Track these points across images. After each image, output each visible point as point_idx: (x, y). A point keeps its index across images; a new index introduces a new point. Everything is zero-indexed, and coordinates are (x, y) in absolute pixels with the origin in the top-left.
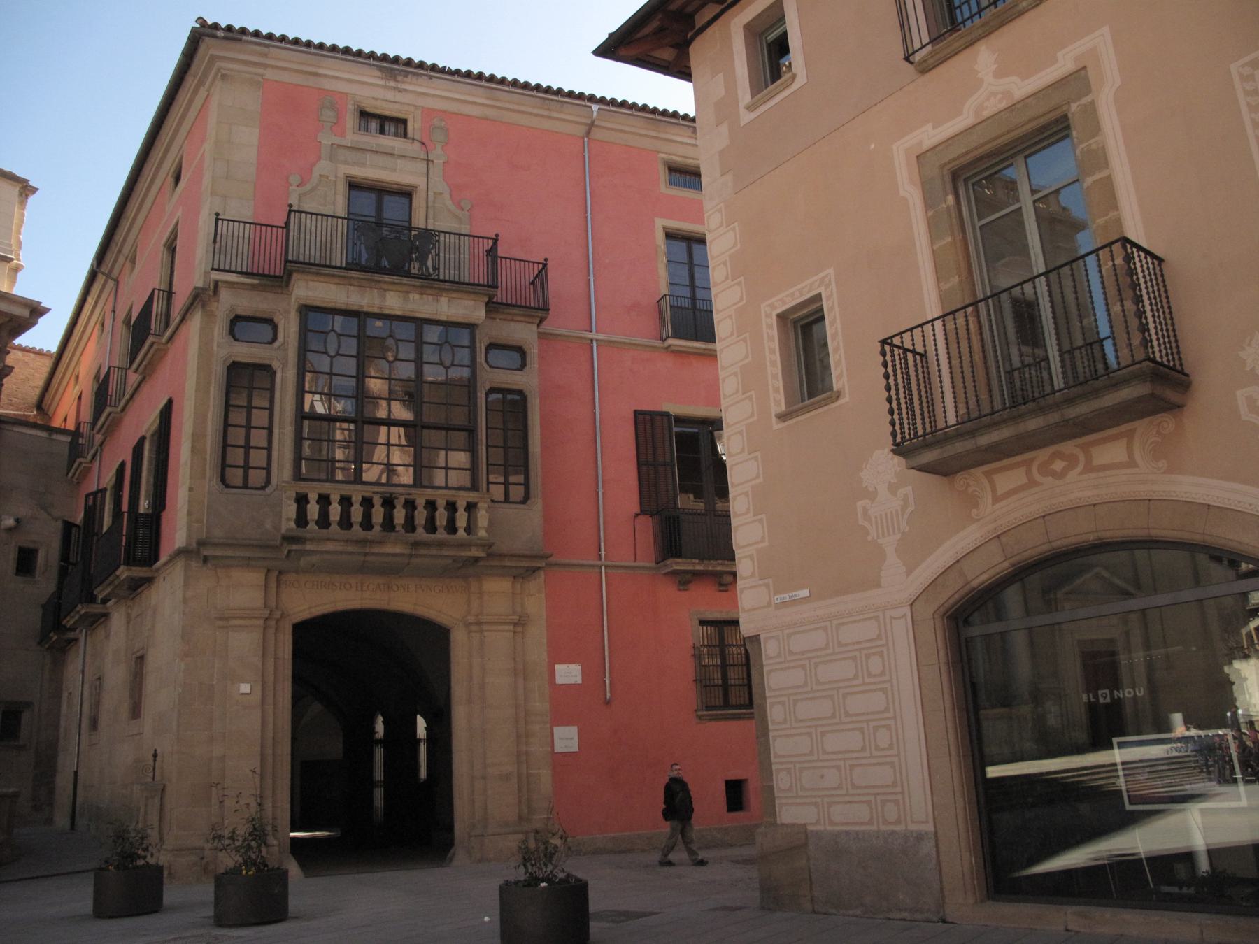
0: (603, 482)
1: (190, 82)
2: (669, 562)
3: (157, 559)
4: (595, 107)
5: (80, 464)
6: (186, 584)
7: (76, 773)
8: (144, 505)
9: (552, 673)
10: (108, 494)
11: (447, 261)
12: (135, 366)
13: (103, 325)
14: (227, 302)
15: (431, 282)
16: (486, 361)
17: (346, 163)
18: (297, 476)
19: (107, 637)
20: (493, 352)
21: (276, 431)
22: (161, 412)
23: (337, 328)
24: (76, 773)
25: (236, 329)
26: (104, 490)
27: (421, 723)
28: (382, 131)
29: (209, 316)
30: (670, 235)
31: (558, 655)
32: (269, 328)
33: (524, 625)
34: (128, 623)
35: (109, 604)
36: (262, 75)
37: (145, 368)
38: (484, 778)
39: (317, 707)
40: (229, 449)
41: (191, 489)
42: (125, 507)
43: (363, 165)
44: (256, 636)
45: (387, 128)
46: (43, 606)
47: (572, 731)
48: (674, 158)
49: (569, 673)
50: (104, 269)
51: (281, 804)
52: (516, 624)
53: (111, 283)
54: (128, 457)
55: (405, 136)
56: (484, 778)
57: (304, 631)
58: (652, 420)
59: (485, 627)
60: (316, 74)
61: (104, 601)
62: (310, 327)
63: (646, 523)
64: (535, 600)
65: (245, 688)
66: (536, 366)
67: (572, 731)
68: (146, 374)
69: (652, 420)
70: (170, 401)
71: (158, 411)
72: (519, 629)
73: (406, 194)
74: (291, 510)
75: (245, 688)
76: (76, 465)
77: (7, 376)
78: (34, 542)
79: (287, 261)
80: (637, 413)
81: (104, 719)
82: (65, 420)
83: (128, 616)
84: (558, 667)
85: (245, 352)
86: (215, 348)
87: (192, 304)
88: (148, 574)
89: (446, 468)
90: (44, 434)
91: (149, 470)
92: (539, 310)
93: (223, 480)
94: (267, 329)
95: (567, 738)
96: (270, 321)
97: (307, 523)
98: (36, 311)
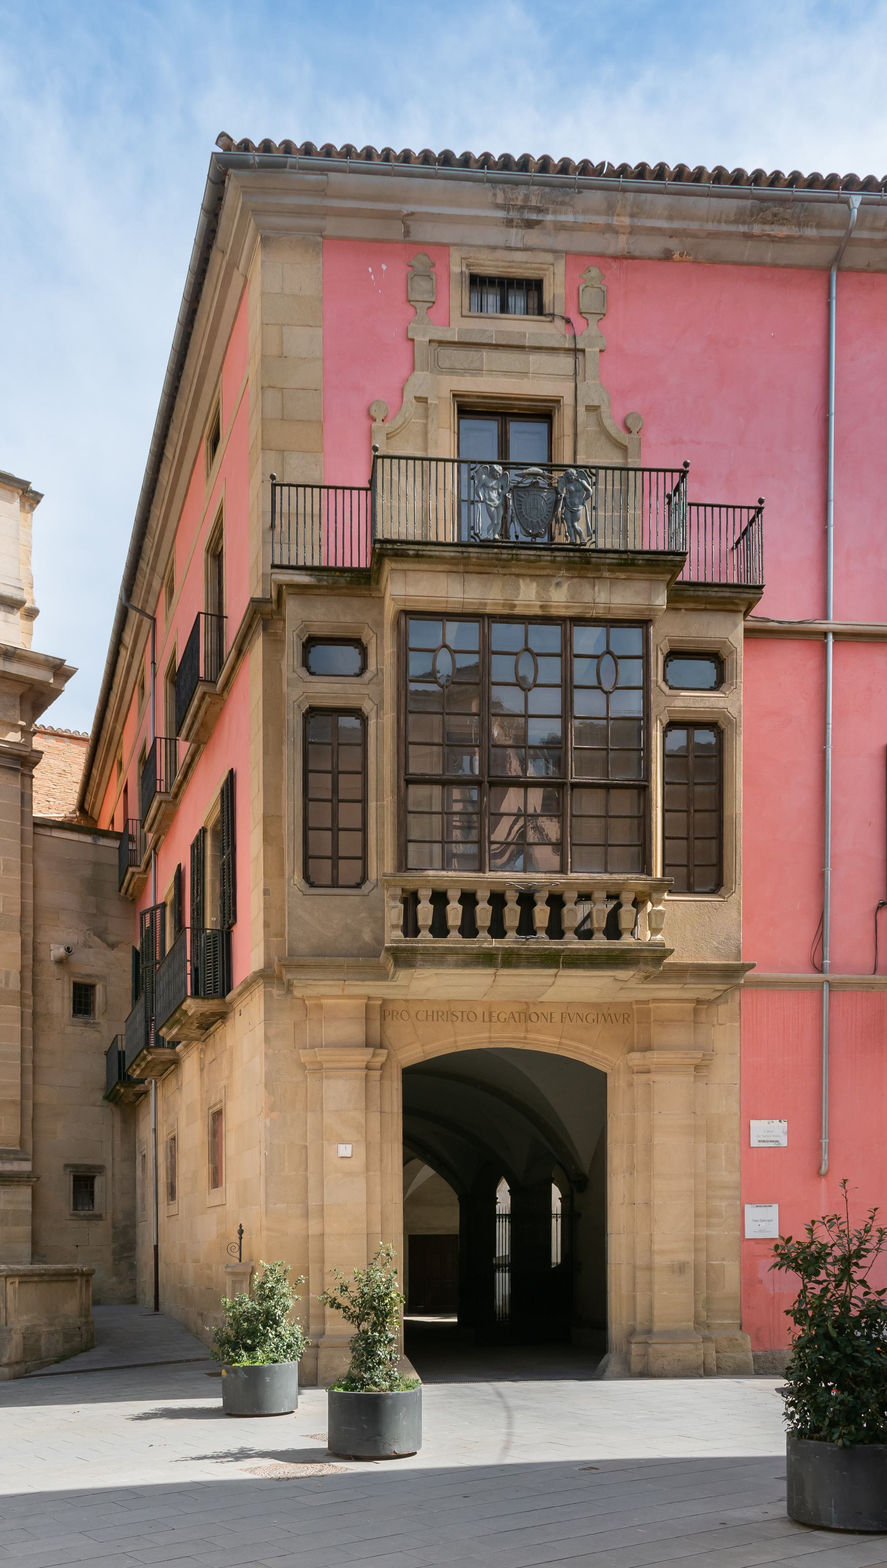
1: (218, 262)
3: (230, 989)
5: (133, 874)
6: (267, 1020)
7: (156, 1248)
8: (211, 920)
10: (168, 909)
12: (184, 732)
13: (143, 687)
14: (298, 616)
16: (665, 680)
17: (452, 371)
18: (402, 865)
19: (179, 1088)
20: (677, 665)
21: (372, 805)
22: (222, 791)
23: (450, 641)
24: (156, 1248)
25: (311, 657)
26: (164, 905)
27: (556, 1193)
28: (504, 308)
29: (275, 641)
31: (749, 1113)
32: (357, 671)
34: (202, 1070)
35: (179, 1048)
37: (197, 734)
39: (426, 1172)
41: (266, 892)
42: (188, 923)
43: (477, 371)
45: (511, 300)
46: (107, 1054)
49: (769, 1132)
50: (137, 602)
51: (394, 1284)
53: (147, 623)
54: (186, 860)
55: (540, 311)
61: (174, 1044)
62: (411, 645)
65: (345, 1150)
68: (202, 740)
70: (232, 775)
71: (218, 792)
73: (542, 413)
74: (394, 913)
75: (345, 1150)
76: (128, 876)
77: (36, 763)
78: (90, 976)
79: (375, 541)
81: (182, 1187)
82: (112, 822)
83: (201, 1061)
84: (754, 1123)
85: (326, 691)
86: (285, 688)
87: (250, 626)
88: (222, 1009)
90: (89, 839)
91: (213, 874)
93: (306, 877)
94: (352, 652)
96: (356, 642)
97: (416, 931)
98: (61, 671)
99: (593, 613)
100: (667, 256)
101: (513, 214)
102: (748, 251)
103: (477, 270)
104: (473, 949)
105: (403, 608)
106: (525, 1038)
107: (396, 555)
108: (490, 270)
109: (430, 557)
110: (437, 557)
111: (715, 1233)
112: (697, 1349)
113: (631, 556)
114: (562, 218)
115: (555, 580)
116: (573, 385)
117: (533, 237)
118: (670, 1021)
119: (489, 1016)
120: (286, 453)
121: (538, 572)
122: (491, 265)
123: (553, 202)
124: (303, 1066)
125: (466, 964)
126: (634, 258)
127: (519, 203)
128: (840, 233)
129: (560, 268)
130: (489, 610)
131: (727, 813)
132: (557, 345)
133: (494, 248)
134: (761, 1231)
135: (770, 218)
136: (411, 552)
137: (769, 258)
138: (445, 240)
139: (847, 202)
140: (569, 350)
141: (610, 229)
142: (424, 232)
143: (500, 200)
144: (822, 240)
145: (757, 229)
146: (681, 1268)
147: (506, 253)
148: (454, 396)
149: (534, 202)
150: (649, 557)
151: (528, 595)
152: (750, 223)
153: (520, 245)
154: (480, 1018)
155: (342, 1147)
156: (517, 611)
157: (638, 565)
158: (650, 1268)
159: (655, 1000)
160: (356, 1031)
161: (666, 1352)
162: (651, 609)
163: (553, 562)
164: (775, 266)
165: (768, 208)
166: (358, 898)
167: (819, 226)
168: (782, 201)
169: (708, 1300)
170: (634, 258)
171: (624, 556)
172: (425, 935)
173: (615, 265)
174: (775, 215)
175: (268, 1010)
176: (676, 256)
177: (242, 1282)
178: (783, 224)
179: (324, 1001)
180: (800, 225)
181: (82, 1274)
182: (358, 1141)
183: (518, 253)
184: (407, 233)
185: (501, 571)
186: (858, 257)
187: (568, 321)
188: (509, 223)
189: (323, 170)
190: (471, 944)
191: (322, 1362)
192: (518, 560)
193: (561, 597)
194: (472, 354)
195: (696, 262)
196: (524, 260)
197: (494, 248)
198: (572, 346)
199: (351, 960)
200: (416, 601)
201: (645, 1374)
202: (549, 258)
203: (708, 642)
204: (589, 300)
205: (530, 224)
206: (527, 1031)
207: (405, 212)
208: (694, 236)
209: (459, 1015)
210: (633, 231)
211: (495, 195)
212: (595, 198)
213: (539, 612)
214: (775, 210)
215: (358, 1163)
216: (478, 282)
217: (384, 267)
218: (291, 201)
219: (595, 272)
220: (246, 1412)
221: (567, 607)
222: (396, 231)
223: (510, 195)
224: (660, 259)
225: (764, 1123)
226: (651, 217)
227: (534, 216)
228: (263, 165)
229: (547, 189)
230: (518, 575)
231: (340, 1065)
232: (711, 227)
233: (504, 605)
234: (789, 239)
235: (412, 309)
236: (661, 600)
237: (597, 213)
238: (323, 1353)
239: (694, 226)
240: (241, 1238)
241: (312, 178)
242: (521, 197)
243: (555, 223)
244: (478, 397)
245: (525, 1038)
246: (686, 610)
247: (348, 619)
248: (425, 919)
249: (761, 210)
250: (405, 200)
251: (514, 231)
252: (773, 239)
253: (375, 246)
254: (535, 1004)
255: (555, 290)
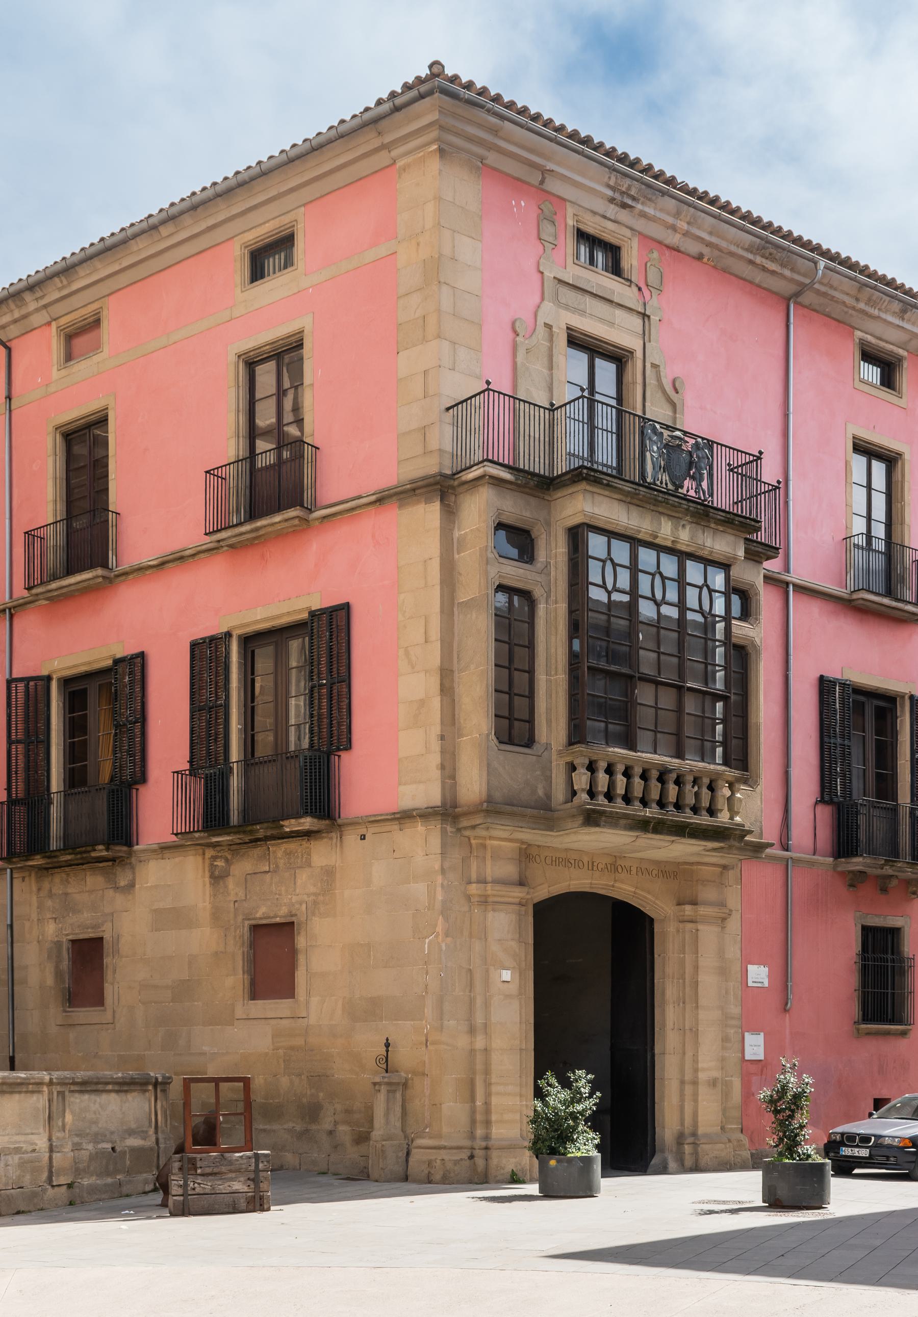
17: (567, 307)
43: (583, 313)
75: (506, 975)
84: (750, 967)
99: (700, 553)
100: (700, 257)
101: (617, 196)
102: (747, 271)
103: (582, 227)
104: (640, 816)
105: (587, 521)
106: (613, 886)
107: (595, 481)
108: (590, 230)
109: (616, 488)
110: (619, 489)
112: (726, 1148)
113: (732, 516)
114: (647, 210)
115: (682, 522)
116: (642, 342)
117: (623, 215)
118: (708, 881)
119: (592, 866)
120: (457, 346)
121: (674, 514)
122: (592, 226)
123: (645, 197)
124: (468, 898)
125: (631, 828)
126: (679, 251)
127: (624, 189)
128: (807, 281)
129: (635, 243)
130: (640, 536)
131: (752, 720)
132: (633, 307)
134: (755, 1054)
135: (767, 255)
136: (605, 482)
137: (757, 281)
138: (565, 197)
139: (816, 263)
141: (674, 228)
142: (554, 186)
143: (612, 183)
144: (792, 280)
145: (758, 260)
147: (602, 220)
148: (568, 328)
149: (633, 192)
150: (741, 519)
151: (666, 530)
152: (755, 254)
153: (612, 218)
154: (586, 866)
155: (504, 972)
156: (657, 541)
157: (734, 524)
158: (695, 1083)
159: (699, 863)
160: (509, 870)
161: (709, 1151)
162: (735, 558)
163: (687, 510)
164: (759, 286)
165: (768, 248)
167: (792, 270)
168: (777, 246)
170: (679, 251)
171: (728, 516)
172: (601, 800)
173: (667, 252)
174: (771, 254)
175: (444, 845)
176: (705, 260)
177: (394, 1091)
178: (773, 261)
179: (488, 842)
180: (783, 265)
181: (156, 1084)
183: (610, 223)
184: (542, 182)
185: (652, 507)
186: (808, 298)
187: (640, 289)
188: (612, 200)
189: (502, 118)
190: (636, 809)
191: (494, 1161)
192: (667, 503)
193: (685, 535)
195: (714, 267)
196: (613, 229)
198: (643, 311)
199: (535, 812)
200: (598, 519)
201: (697, 1168)
202: (628, 233)
203: (743, 583)
204: (653, 278)
205: (624, 206)
206: (615, 881)
207: (548, 168)
208: (720, 250)
209: (573, 862)
210: (686, 234)
211: (610, 178)
212: (671, 204)
213: (669, 544)
214: (772, 251)
216: (582, 236)
217: (523, 204)
218: (471, 130)
219: (655, 255)
220: (581, 1194)
221: (688, 545)
222: (534, 178)
223: (619, 181)
224: (694, 258)
225: (756, 967)
226: (699, 228)
227: (630, 202)
229: (643, 187)
230: (661, 513)
231: (506, 900)
232: (733, 248)
233: (651, 535)
234: (773, 273)
235: (541, 247)
236: (741, 553)
237: (668, 214)
238: (494, 1154)
239: (723, 244)
240: (387, 1051)
241: (493, 120)
242: (626, 186)
243: (641, 211)
244: (582, 333)
245: (613, 886)
247: (527, 514)
248: (603, 787)
249: (764, 248)
250: (548, 158)
251: (612, 206)
252: (764, 269)
253: (518, 184)
254: (620, 858)
255: (631, 259)
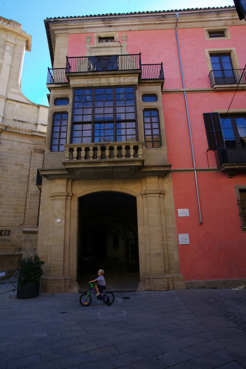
0: (192, 140)
2: (223, 165)
4: (177, 13)
9: (177, 213)
11: (124, 64)
15: (117, 72)
30: (212, 55)
31: (177, 207)
33: (164, 194)
36: (68, 33)
38: (150, 255)
40: (53, 140)
44: (63, 202)
47: (186, 236)
48: (210, 28)
49: (184, 212)
52: (160, 194)
56: (150, 255)
57: (82, 200)
58: (225, 83)
59: (148, 195)
60: (83, 28)
63: (212, 154)
64: (167, 185)
66: (161, 99)
67: (186, 236)
69: (225, 83)
72: (162, 196)
74: (67, 154)
80: (203, 114)
84: (179, 210)
89: (126, 135)
92: (160, 81)
95: (184, 239)
111: (170, 243)
133: (103, 32)
140: (120, 46)
146: (159, 255)
166: (63, 153)
169: (169, 264)
182: (63, 218)
194: (99, 49)
197: (103, 32)
202: (115, 33)
215: (62, 224)
225: (182, 210)
228: (54, 21)
246: (146, 86)
247: (65, 93)
